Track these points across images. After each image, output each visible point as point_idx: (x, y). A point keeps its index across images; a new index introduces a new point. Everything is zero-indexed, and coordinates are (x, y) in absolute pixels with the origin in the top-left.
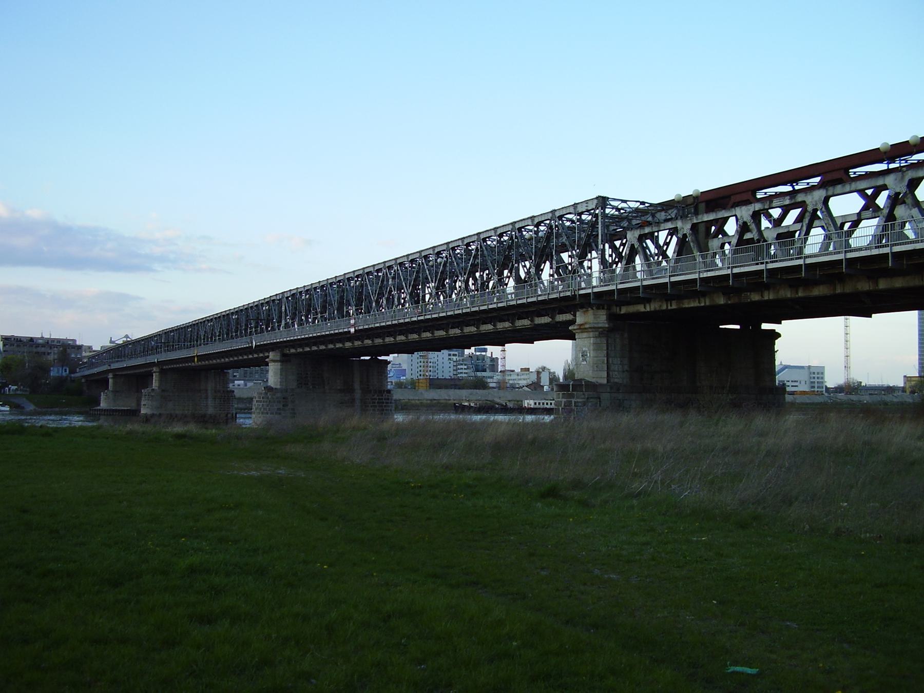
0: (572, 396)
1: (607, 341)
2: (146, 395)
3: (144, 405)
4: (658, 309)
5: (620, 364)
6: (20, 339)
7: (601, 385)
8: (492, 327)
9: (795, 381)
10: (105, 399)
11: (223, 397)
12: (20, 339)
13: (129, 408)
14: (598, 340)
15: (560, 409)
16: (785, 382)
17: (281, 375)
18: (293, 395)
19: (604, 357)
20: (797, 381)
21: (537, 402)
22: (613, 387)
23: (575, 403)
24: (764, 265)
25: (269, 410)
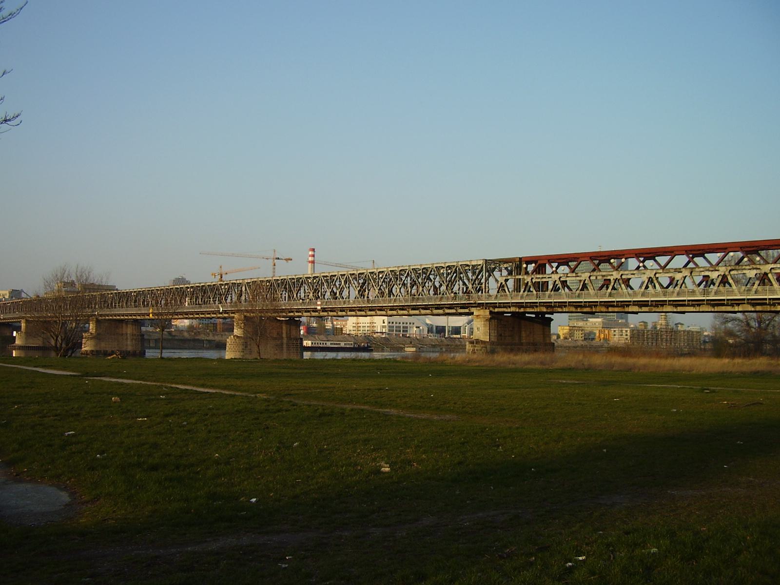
0: (475, 346)
4: (514, 311)
7: (487, 342)
13: (37, 345)
21: (314, 342)
22: (491, 343)
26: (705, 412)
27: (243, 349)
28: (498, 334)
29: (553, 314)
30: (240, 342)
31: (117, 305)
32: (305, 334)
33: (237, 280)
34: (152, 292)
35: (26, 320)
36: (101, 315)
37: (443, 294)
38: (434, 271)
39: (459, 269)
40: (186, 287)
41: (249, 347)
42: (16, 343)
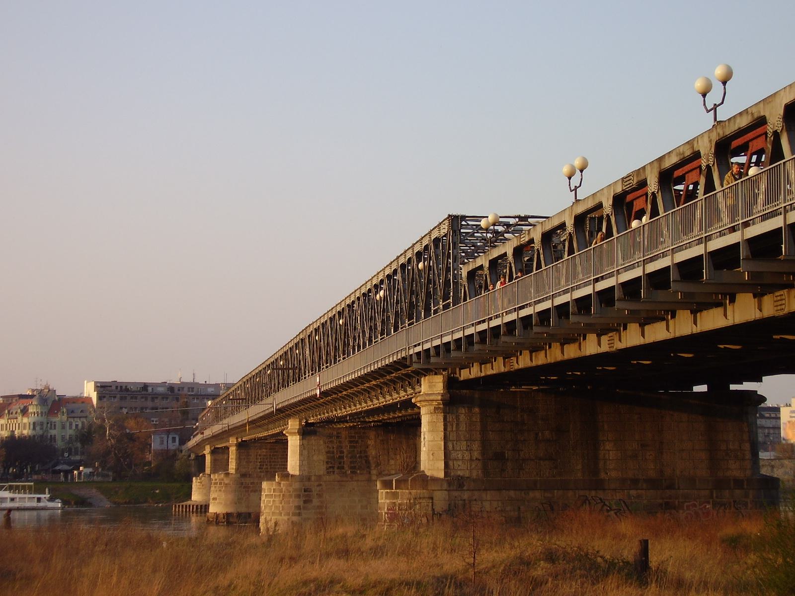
1: (445, 419)
5: (467, 450)
6: (126, 387)
12: (126, 387)
14: (435, 417)
15: (384, 514)
17: (301, 454)
18: (320, 485)
19: (442, 441)
23: (399, 508)
24: (487, 323)
26: (334, 574)
27: (299, 507)
28: (484, 452)
30: (291, 489)
32: (63, 506)
41: (316, 502)
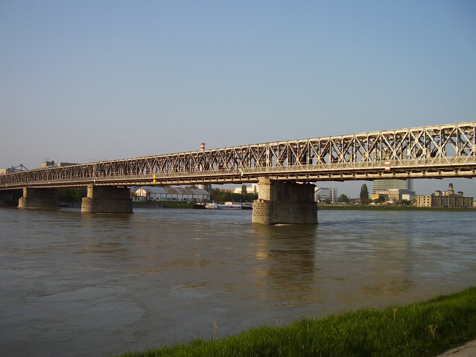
2: (85, 201)
3: (83, 207)
8: (423, 174)
9: (325, 196)
10: (22, 202)
11: (127, 203)
16: (320, 196)
20: (325, 196)
25: (265, 214)
29: (343, 181)
31: (90, 174)
33: (90, 163)
34: (78, 168)
35: (27, 188)
36: (99, 182)
37: (257, 167)
38: (219, 153)
39: (289, 146)
40: (105, 163)
41: (275, 211)
42: (19, 206)
